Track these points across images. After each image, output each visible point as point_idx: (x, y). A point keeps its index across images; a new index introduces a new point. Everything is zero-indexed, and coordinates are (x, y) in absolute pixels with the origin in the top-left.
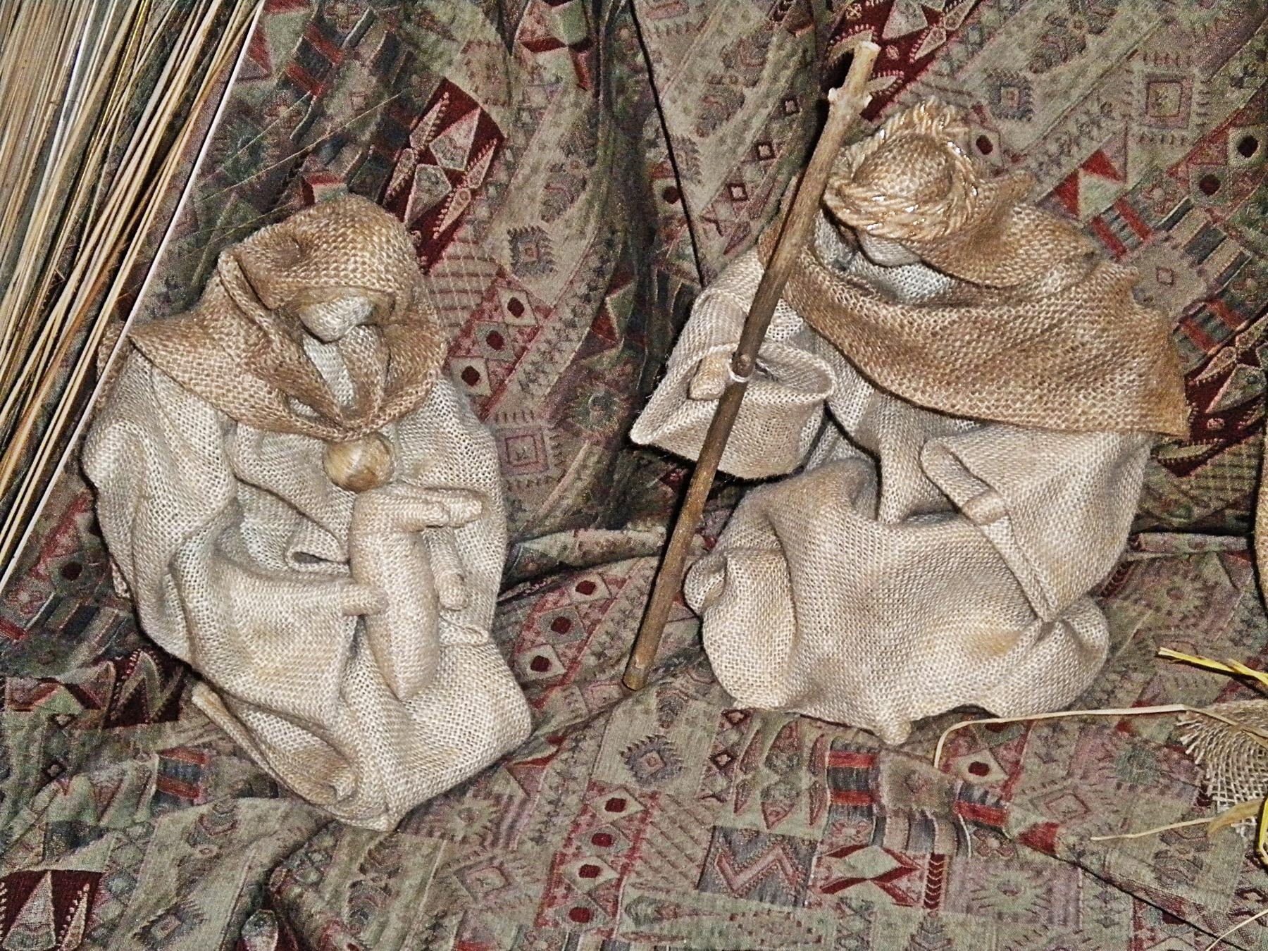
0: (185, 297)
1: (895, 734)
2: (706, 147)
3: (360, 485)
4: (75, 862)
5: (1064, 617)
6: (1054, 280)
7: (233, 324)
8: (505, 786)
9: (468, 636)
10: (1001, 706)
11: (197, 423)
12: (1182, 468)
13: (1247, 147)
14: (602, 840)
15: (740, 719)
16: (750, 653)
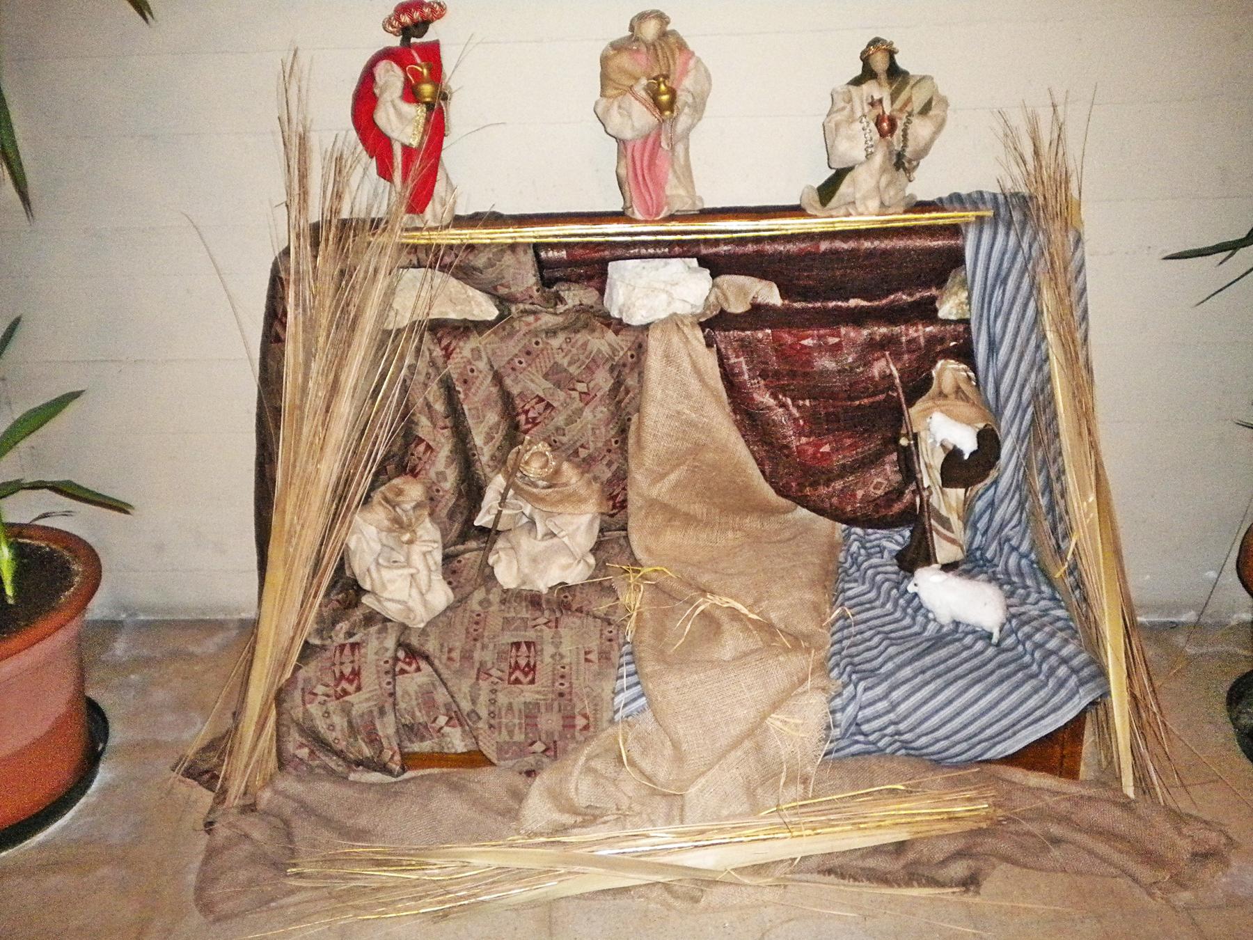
0: (367, 500)
1: (545, 591)
2: (486, 449)
3: (410, 542)
4: (352, 640)
5: (583, 558)
6: (573, 481)
7: (381, 508)
8: (449, 614)
9: (438, 578)
10: (570, 582)
11: (371, 531)
12: (612, 516)
13: (616, 442)
14: (477, 623)
15: (506, 591)
16: (507, 573)
